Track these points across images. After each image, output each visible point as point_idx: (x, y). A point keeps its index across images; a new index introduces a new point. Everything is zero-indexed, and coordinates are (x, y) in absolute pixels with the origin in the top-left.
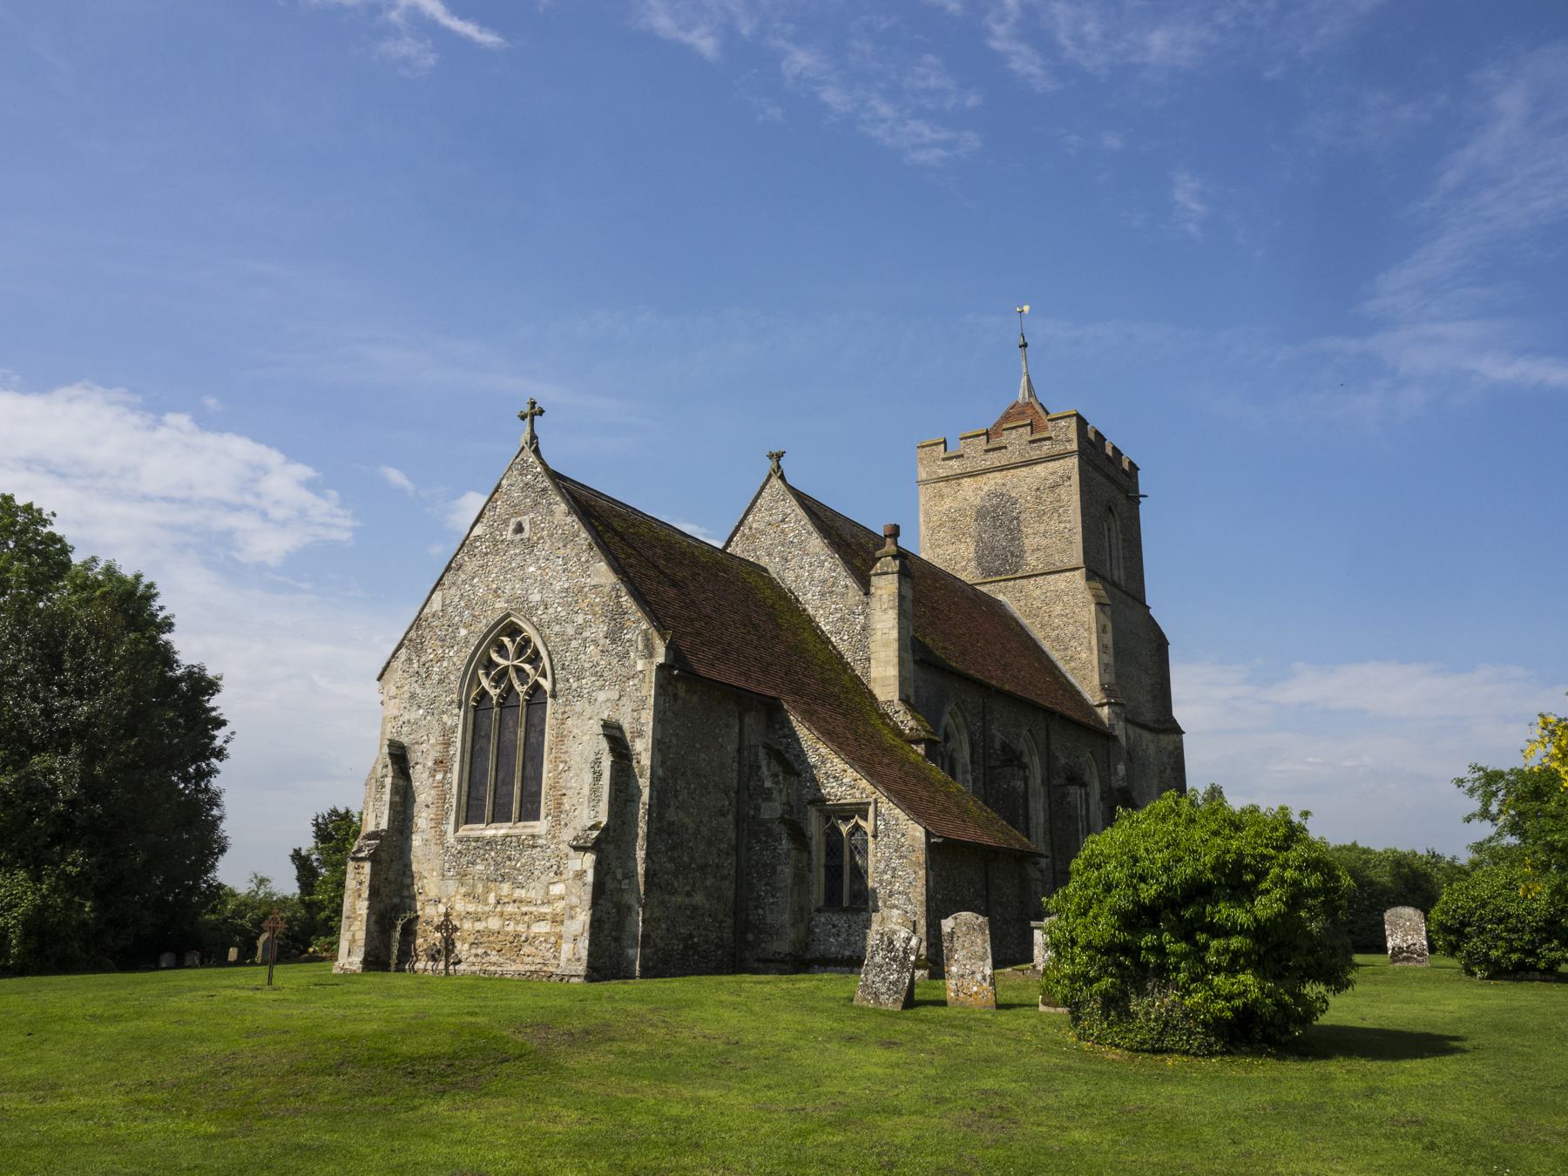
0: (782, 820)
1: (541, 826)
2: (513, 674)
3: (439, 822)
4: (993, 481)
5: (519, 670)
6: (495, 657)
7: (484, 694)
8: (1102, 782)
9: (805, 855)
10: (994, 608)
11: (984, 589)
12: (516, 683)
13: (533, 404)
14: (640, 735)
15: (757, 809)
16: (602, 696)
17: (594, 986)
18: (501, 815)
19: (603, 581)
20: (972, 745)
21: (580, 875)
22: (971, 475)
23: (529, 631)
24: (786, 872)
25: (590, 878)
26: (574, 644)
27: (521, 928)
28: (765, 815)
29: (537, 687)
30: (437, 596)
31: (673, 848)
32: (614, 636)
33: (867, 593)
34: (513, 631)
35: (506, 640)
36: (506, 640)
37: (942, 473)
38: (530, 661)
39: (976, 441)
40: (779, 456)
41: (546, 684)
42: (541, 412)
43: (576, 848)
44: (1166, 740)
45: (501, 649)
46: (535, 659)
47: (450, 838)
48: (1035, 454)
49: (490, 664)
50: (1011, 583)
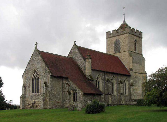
0: (68, 92)
1: (39, 93)
2: (36, 76)
3: (29, 93)
4: (116, 38)
5: (36, 76)
6: (34, 74)
7: (33, 78)
8: (128, 82)
9: (71, 95)
10: (117, 58)
11: (114, 55)
12: (36, 77)
13: (36, 43)
14: (49, 83)
15: (65, 90)
16: (45, 79)
17: (90, 116)
18: (35, 92)
19: (44, 65)
20: (102, 80)
21: (42, 99)
22: (113, 37)
23: (37, 71)
24: (68, 97)
25: (43, 99)
26: (42, 73)
27: (38, 104)
28: (66, 91)
29: (38, 78)
30: (27, 67)
31: (53, 95)
32: (45, 72)
33: (85, 61)
34: (35, 71)
35: (35, 72)
36: (35, 72)
37: (110, 37)
38: (37, 75)
39: (114, 31)
40: (75, 42)
41: (39, 77)
42: (37, 44)
43: (42, 96)
44: (144, 75)
45: (35, 73)
46: (38, 75)
47: (30, 95)
48: (123, 33)
49: (34, 75)
50: (119, 53)
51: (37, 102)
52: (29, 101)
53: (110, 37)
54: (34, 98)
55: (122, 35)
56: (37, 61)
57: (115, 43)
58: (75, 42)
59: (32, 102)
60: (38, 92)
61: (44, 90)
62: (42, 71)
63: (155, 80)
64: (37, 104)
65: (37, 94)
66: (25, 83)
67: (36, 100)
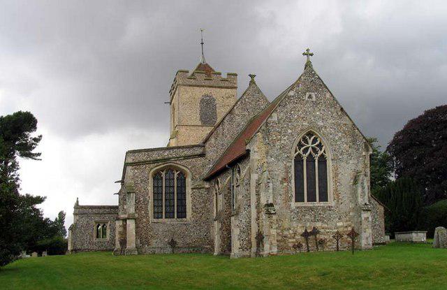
16: (351, 162)
18: (312, 198)
22: (198, 86)
25: (370, 219)
51: (322, 231)
52: (286, 226)
53: (190, 86)
54: (308, 217)
55: (219, 87)
56: (315, 104)
57: (202, 101)
58: (252, 76)
59: (301, 231)
60: (324, 197)
61: (364, 192)
62: (340, 138)
63: (392, 178)
64: (322, 237)
65: (317, 204)
66: (265, 165)
67: (319, 225)
